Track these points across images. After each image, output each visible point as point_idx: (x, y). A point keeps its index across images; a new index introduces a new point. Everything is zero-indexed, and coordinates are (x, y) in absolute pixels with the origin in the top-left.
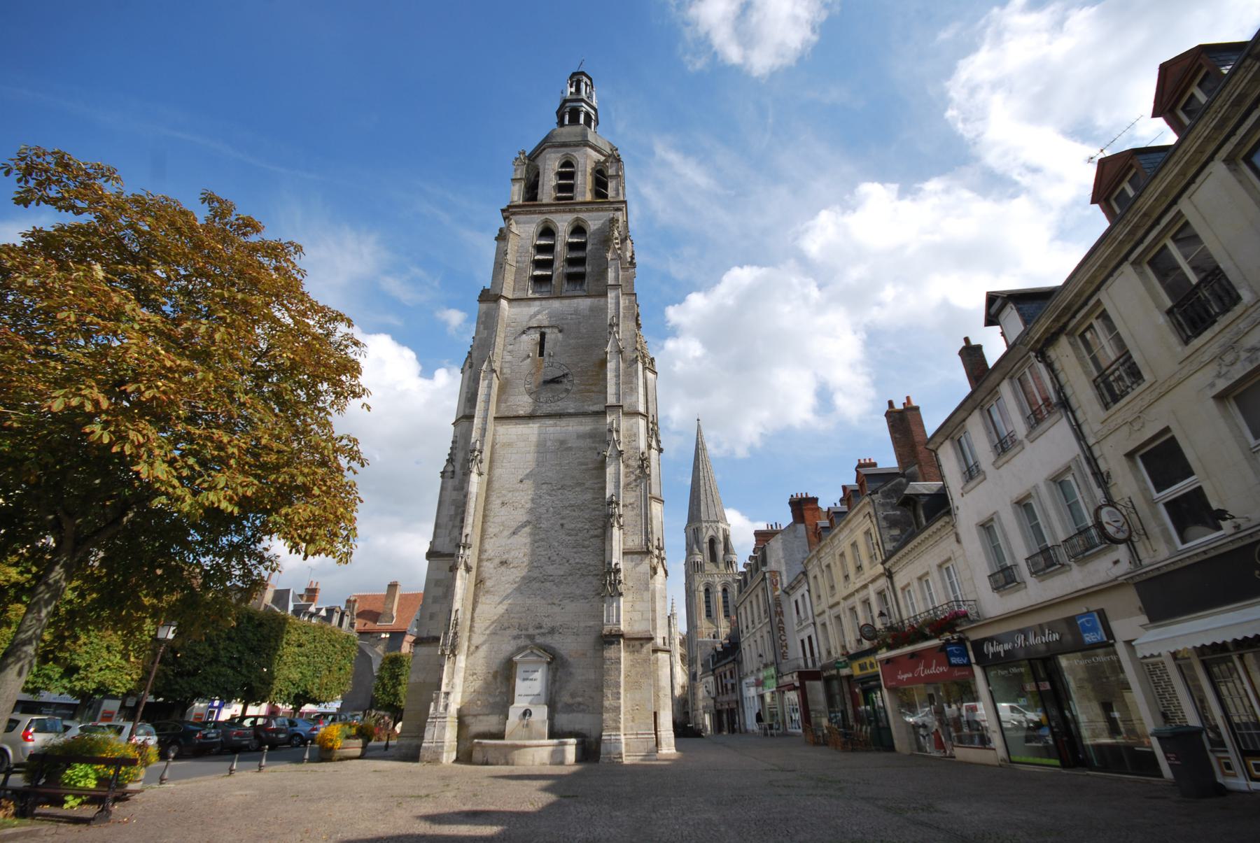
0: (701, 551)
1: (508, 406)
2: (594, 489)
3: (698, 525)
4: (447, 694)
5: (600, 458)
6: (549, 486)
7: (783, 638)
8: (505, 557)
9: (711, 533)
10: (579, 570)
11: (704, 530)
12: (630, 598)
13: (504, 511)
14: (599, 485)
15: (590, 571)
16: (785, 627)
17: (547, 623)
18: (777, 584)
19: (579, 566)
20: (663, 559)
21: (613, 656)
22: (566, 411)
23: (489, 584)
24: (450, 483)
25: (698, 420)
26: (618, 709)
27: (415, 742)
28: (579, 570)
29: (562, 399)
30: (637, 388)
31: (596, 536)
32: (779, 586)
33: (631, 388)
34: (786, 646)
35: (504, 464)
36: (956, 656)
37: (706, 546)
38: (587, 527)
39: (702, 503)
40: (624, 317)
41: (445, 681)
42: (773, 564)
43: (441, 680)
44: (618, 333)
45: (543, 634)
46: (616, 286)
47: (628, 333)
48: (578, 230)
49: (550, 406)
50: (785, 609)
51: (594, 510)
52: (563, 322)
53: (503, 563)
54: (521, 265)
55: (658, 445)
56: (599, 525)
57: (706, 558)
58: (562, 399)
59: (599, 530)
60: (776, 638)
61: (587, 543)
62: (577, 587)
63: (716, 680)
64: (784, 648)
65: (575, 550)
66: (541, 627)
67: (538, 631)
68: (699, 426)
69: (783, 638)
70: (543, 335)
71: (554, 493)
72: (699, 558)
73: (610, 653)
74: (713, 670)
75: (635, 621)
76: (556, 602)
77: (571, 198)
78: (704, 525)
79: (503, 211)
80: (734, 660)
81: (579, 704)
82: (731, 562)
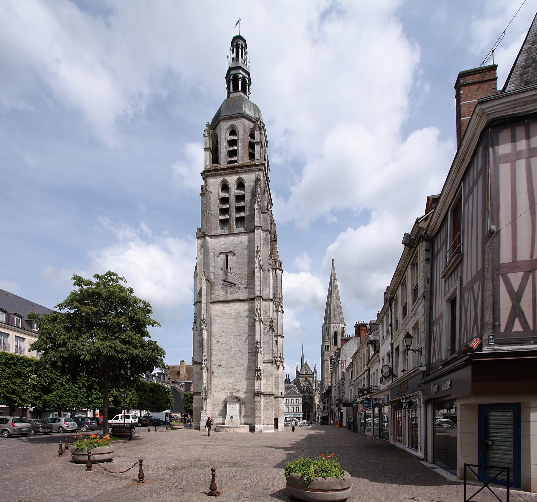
1: (215, 296)
3: (329, 325)
4: (206, 411)
5: (253, 321)
6: (234, 334)
7: (343, 389)
8: (220, 364)
9: (335, 330)
12: (265, 380)
13: (218, 345)
17: (237, 388)
20: (282, 362)
21: (259, 400)
22: (239, 298)
23: (215, 374)
24: (196, 333)
25: (333, 260)
26: (260, 417)
27: (198, 425)
29: (237, 292)
30: (269, 286)
31: (253, 355)
32: (345, 367)
33: (267, 285)
34: (344, 393)
35: (216, 324)
36: (366, 404)
37: (332, 337)
40: (264, 244)
41: (204, 407)
42: (343, 357)
43: (203, 407)
44: (260, 256)
45: (236, 392)
46: (260, 227)
47: (265, 255)
48: (241, 185)
49: (232, 296)
53: (220, 366)
55: (282, 310)
58: (237, 292)
60: (340, 389)
63: (323, 404)
64: (343, 394)
65: (245, 361)
66: (235, 390)
67: (233, 391)
68: (333, 263)
69: (343, 389)
70: (227, 257)
71: (236, 337)
72: (327, 344)
73: (257, 399)
75: (267, 388)
76: (239, 381)
77: (236, 161)
78: (332, 325)
80: (329, 396)
81: (249, 415)
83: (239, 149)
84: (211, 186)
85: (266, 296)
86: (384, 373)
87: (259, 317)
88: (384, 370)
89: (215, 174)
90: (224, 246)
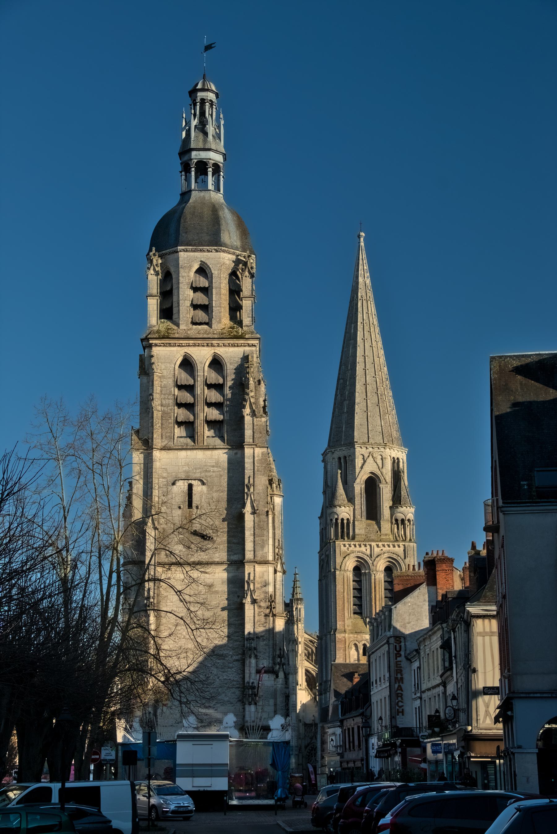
0: (351, 499)
2: (235, 625)
7: (400, 704)
9: (370, 467)
10: (226, 684)
11: (359, 462)
14: (239, 622)
15: (234, 685)
16: (404, 693)
18: (400, 650)
19: (226, 681)
28: (226, 684)
32: (402, 653)
37: (359, 487)
38: (231, 653)
39: (357, 409)
50: (406, 676)
51: (236, 641)
52: (207, 474)
54: (165, 409)
56: (240, 652)
57: (358, 512)
59: (240, 656)
60: (393, 704)
61: (231, 665)
62: (225, 695)
63: (344, 732)
65: (223, 670)
70: (190, 487)
74: (342, 721)
79: (142, 340)
82: (403, 521)
83: (214, 305)
84: (162, 363)
85: (261, 558)
86: (447, 716)
87: (251, 595)
88: (447, 712)
89: (170, 344)
90: (186, 468)
